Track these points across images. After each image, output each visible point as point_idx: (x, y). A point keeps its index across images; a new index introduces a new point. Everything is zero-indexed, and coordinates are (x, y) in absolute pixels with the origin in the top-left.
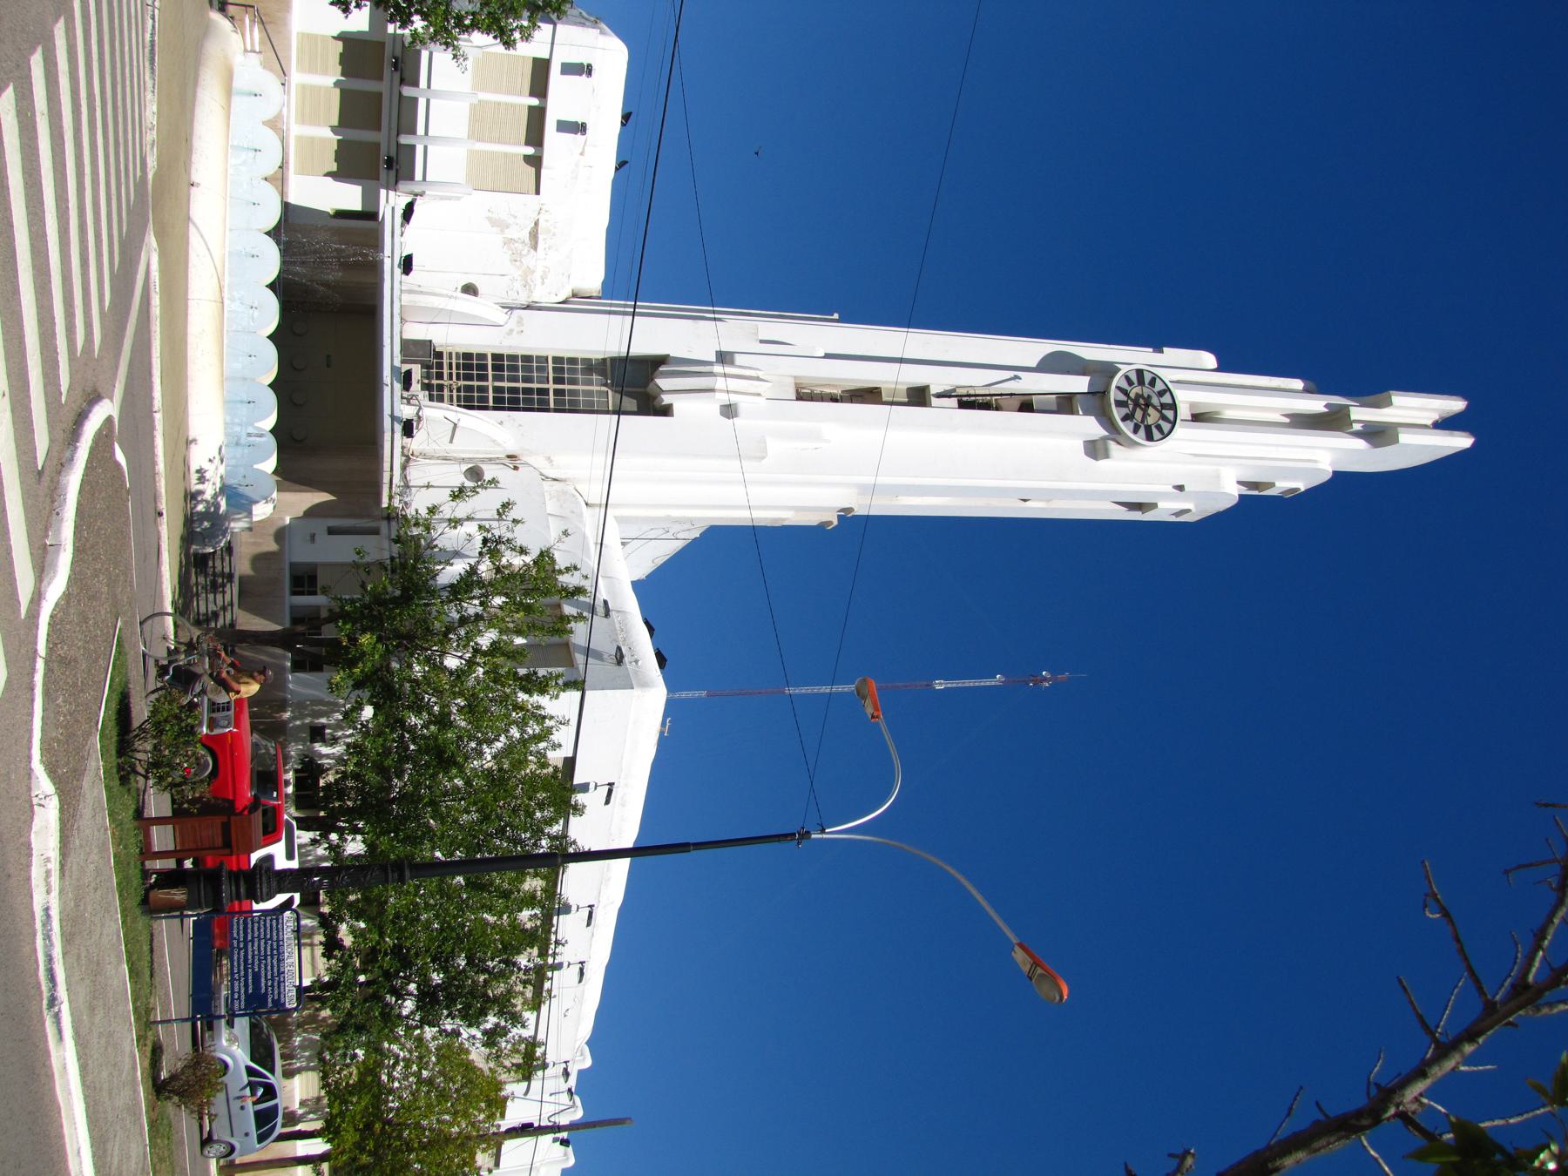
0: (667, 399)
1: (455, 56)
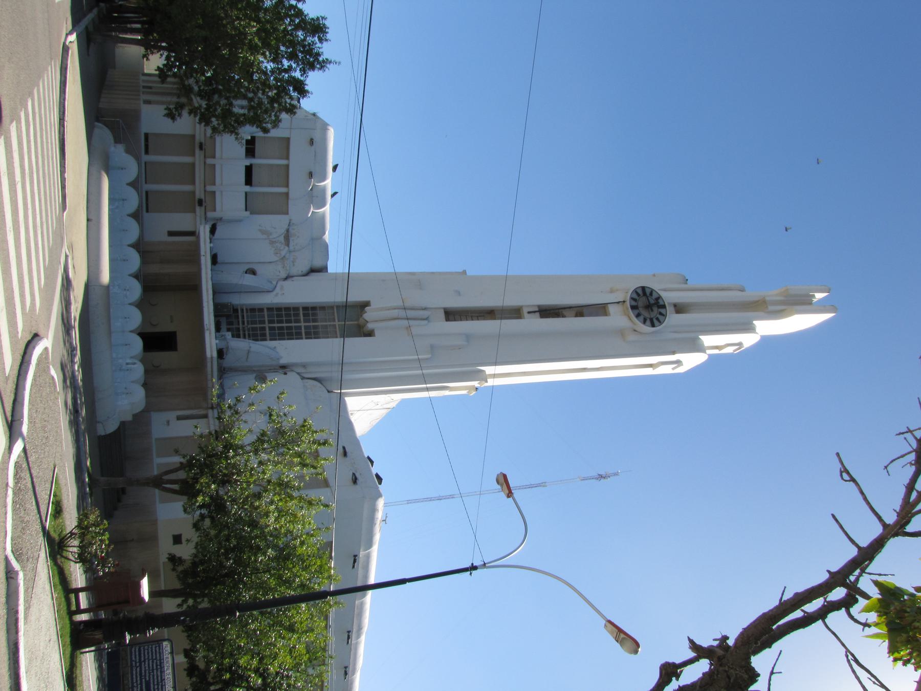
0: (370, 326)
1: (236, 138)
